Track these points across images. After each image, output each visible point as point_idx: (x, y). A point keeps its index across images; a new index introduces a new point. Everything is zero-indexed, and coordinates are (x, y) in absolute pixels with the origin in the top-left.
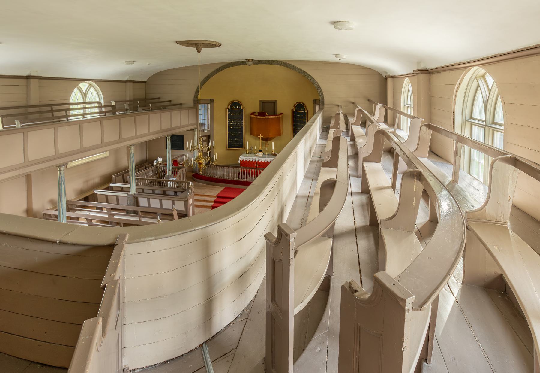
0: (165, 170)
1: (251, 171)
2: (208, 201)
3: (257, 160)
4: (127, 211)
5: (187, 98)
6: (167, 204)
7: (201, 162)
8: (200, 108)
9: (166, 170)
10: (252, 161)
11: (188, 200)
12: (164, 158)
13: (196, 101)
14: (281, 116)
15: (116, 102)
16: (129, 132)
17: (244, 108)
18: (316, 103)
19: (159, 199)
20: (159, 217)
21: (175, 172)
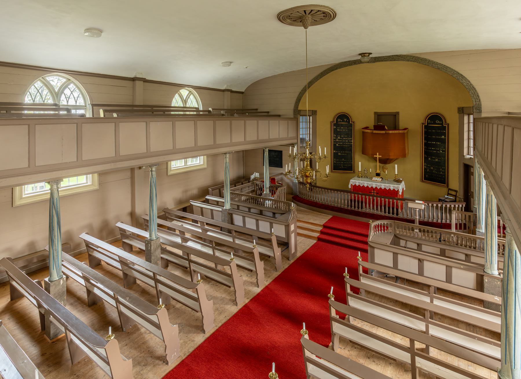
0: (262, 188)
1: (368, 199)
2: (313, 231)
3: (374, 186)
4: (221, 229)
5: (288, 109)
6: (264, 227)
7: (307, 174)
8: (301, 120)
9: (263, 187)
10: (368, 187)
11: (289, 224)
12: (262, 175)
13: (297, 113)
14: (406, 131)
15: (213, 109)
16: (223, 138)
17: (354, 122)
18: (463, 112)
19: (255, 219)
20: (254, 240)
21: (273, 191)
